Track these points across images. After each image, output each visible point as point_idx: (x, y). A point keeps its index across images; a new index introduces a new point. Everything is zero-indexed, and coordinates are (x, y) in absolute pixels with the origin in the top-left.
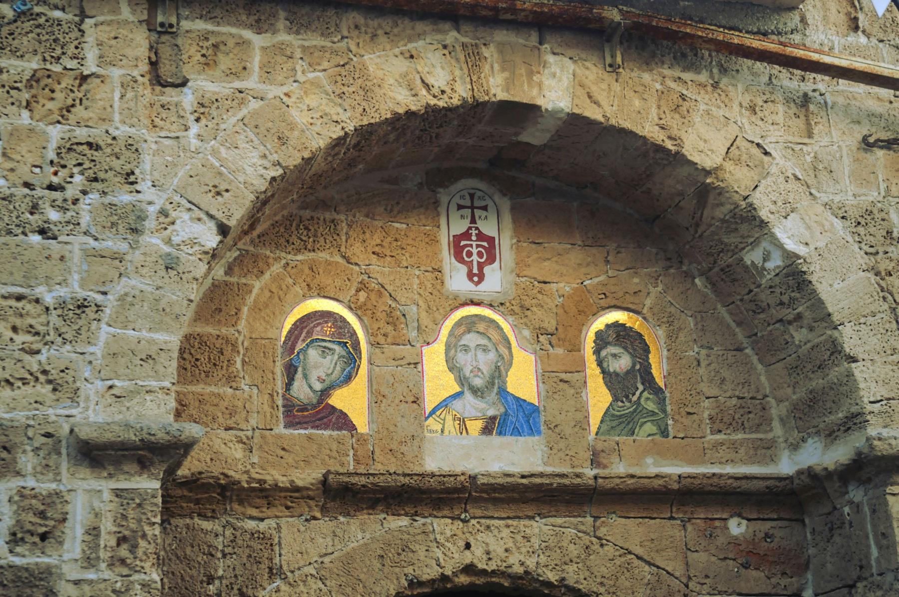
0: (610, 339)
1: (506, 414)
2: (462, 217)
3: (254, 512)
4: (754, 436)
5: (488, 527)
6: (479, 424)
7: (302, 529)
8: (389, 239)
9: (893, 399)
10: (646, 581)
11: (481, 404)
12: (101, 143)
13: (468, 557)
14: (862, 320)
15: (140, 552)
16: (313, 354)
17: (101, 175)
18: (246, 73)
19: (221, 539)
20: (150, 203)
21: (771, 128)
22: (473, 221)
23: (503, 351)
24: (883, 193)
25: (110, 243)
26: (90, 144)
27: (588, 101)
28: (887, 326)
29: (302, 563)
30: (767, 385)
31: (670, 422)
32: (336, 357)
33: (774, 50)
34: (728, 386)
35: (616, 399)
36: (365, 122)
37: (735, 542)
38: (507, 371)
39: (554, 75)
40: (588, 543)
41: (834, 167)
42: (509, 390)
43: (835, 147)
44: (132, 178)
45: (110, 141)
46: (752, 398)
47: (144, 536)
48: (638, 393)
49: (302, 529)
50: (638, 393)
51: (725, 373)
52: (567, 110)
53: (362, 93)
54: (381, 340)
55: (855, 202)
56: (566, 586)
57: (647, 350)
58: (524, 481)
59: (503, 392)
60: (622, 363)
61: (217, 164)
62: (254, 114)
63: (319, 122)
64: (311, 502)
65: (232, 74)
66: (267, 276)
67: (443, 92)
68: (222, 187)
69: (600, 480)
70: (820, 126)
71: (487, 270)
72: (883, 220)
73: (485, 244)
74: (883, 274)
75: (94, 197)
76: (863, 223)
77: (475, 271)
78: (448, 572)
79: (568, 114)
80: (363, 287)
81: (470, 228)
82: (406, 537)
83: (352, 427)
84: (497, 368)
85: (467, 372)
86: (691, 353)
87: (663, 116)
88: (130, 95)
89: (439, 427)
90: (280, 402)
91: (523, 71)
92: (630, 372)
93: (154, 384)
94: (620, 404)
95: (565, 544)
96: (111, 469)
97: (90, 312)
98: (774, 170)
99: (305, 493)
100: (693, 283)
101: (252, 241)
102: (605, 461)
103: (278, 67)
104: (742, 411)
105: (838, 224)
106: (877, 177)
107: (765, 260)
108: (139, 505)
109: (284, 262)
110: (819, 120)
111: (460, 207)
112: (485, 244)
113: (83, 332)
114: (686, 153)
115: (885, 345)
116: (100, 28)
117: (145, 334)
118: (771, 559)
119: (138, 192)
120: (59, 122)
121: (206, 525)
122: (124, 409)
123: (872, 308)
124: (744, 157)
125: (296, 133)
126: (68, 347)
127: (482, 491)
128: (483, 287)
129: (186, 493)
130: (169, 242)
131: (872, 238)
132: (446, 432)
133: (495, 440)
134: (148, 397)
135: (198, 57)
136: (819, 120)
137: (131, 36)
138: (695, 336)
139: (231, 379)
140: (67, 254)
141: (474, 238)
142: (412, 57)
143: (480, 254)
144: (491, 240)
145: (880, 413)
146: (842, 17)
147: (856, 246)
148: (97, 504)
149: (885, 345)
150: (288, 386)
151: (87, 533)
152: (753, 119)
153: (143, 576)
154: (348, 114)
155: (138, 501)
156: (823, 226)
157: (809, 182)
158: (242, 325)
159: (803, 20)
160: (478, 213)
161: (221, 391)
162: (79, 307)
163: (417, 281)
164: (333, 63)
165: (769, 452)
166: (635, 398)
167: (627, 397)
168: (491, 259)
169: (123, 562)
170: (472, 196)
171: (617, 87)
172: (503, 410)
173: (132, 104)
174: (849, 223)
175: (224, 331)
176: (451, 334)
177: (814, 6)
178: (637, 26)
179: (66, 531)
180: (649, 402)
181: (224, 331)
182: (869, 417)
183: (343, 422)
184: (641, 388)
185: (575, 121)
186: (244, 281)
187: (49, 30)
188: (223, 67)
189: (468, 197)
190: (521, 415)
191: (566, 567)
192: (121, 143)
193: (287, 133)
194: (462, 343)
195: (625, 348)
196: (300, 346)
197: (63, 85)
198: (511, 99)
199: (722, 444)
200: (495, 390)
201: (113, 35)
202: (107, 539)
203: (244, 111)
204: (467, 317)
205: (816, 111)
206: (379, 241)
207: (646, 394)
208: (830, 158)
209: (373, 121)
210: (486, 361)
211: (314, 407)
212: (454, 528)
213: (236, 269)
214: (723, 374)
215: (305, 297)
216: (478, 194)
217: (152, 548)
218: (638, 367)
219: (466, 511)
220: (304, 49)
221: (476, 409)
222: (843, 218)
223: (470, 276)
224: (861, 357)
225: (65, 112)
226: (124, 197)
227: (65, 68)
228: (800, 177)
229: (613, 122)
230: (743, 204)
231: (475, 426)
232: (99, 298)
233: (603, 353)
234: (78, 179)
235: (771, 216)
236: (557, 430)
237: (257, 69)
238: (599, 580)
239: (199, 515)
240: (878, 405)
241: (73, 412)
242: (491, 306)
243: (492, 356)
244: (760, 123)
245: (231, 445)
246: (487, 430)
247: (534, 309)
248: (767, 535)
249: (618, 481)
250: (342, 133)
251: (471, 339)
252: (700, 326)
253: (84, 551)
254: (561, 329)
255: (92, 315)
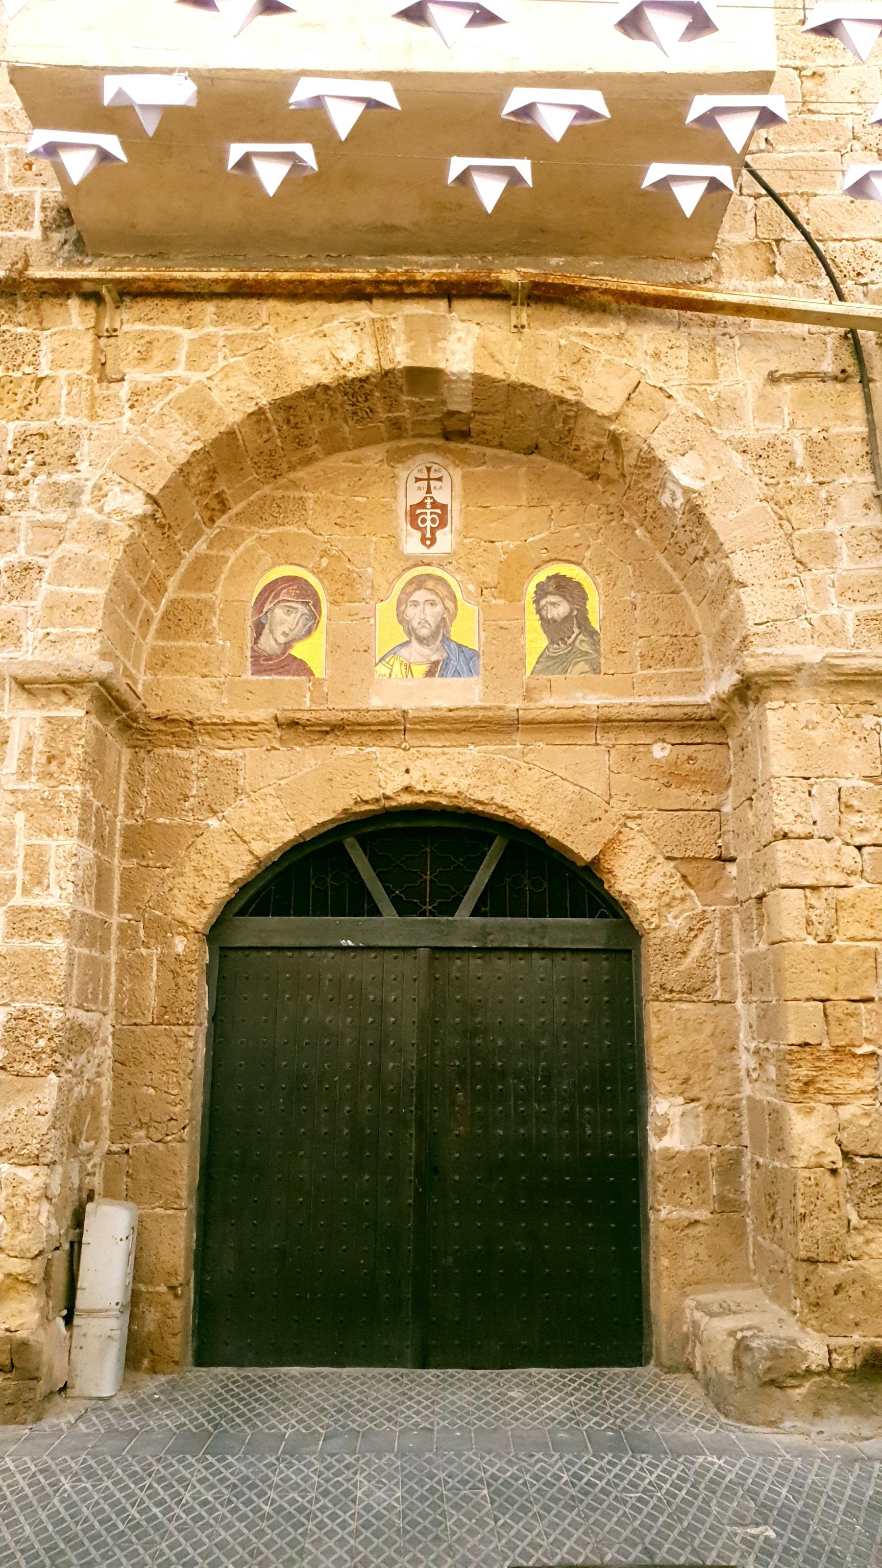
0: (551, 589)
1: (448, 658)
2: (419, 488)
3: (221, 743)
4: (683, 670)
5: (426, 755)
6: (425, 668)
7: (264, 757)
8: (350, 512)
9: (781, 620)
10: (568, 799)
11: (426, 651)
12: (50, 433)
13: (406, 780)
14: (756, 547)
15: (66, 768)
16: (279, 612)
17: (48, 460)
18: (175, 363)
19: (195, 765)
20: (87, 480)
21: (675, 372)
22: (429, 491)
23: (449, 604)
24: (787, 426)
25: (51, 515)
26: (41, 435)
27: (490, 360)
28: (782, 551)
29: (262, 785)
30: (700, 624)
31: (602, 661)
32: (299, 614)
33: (666, 294)
34: (661, 626)
35: (552, 642)
36: (277, 397)
37: (657, 765)
38: (451, 622)
39: (459, 339)
40: (516, 767)
41: (738, 404)
42: (453, 638)
43: (740, 386)
44: (73, 461)
45: (57, 431)
46: (685, 636)
47: (69, 755)
48: (574, 636)
49: (264, 757)
50: (574, 636)
51: (659, 614)
52: (471, 371)
53: (276, 370)
54: (339, 598)
55: (757, 436)
56: (496, 804)
57: (584, 597)
58: (451, 714)
59: (446, 639)
60: (560, 609)
61: (145, 443)
62: (180, 397)
63: (237, 400)
64: (269, 735)
65: (163, 366)
66: (241, 548)
67: (351, 364)
68: (148, 463)
69: (521, 712)
70: (726, 367)
71: (439, 534)
72: (786, 451)
73: (439, 511)
74: (782, 502)
75: (42, 478)
76: (764, 455)
77: (428, 535)
78: (389, 793)
79: (473, 375)
80: (325, 553)
81: (426, 498)
82: (352, 763)
83: (309, 672)
84: (443, 619)
85: (415, 624)
86: (629, 598)
87: (564, 369)
88: (74, 391)
89: (388, 671)
90: (249, 653)
91: (428, 339)
92: (567, 618)
93: (82, 630)
94: (555, 646)
95: (494, 768)
96: (43, 700)
97: (33, 574)
98: (673, 410)
99: (261, 726)
100: (633, 533)
101: (230, 519)
102: (536, 696)
103: (203, 356)
104: (673, 648)
105: (738, 458)
106: (782, 412)
107: (673, 500)
108: (67, 730)
109: (257, 535)
110: (726, 360)
111: (418, 480)
112: (439, 511)
113: (27, 589)
114: (585, 402)
115: (776, 569)
116: (54, 337)
117: (76, 589)
118: (692, 779)
119: (78, 471)
120: (17, 419)
121: (183, 754)
122: (57, 652)
123: (767, 535)
124: (647, 402)
125: (215, 411)
126: (14, 602)
127: (415, 723)
128: (433, 549)
129: (162, 728)
130: (100, 511)
131: (773, 470)
132: (393, 676)
133: (437, 680)
134: (78, 642)
135: (135, 353)
136: (726, 360)
137: (78, 341)
138: (632, 582)
139: (208, 635)
140: (17, 526)
141: (429, 506)
142: (325, 336)
143: (433, 521)
144: (443, 507)
145: (764, 634)
146: (761, 264)
147: (757, 478)
148: (32, 728)
149: (776, 569)
150: (256, 640)
151: (23, 752)
152: (657, 365)
153: (67, 787)
154: (263, 391)
155: (65, 727)
156: (721, 460)
157: (711, 420)
158: (219, 590)
159: (718, 270)
160: (433, 484)
161: (199, 645)
162: (26, 569)
163: (373, 546)
164: (253, 347)
165: (698, 683)
166: (570, 641)
167: (562, 639)
168: (443, 524)
169: (51, 775)
170: (429, 469)
171: (519, 345)
172: (446, 655)
173: (76, 398)
174: (749, 456)
175: (204, 596)
176: (403, 591)
177: (730, 255)
178: (536, 285)
179: (8, 751)
180: (584, 644)
181: (204, 596)
182: (752, 639)
183: (302, 668)
184: (576, 631)
185: (481, 381)
186: (221, 553)
187: (12, 343)
188: (156, 361)
189: (425, 470)
190: (462, 658)
191: (494, 788)
192: (66, 430)
193: (207, 412)
194: (412, 598)
195: (564, 597)
196: (267, 606)
197: (23, 387)
198: (415, 365)
199: (651, 678)
200: (440, 638)
201: (64, 342)
202: (38, 758)
203: (172, 395)
204: (419, 576)
205: (722, 353)
206: (341, 514)
207: (581, 636)
208: (734, 396)
209: (284, 395)
210: (432, 614)
211: (278, 657)
212: (395, 755)
213: (216, 543)
214: (658, 616)
215: (274, 566)
216: (435, 467)
217: (76, 765)
218: (575, 613)
219: (405, 740)
220: (227, 337)
221: (421, 655)
222: (744, 452)
223: (423, 540)
224: (749, 582)
225: (23, 411)
226: (64, 477)
227: (24, 374)
228: (702, 416)
229: (513, 378)
230: (645, 447)
231: (420, 670)
232: (41, 561)
233: (543, 602)
234: (30, 464)
235: (669, 455)
236: (493, 672)
237: (183, 359)
238: (524, 798)
239: (177, 746)
240: (764, 626)
241: (16, 655)
242: (440, 566)
243: (439, 608)
244: (663, 368)
245: (205, 689)
246: (430, 673)
247: (480, 566)
248: (690, 758)
249: (538, 712)
250: (256, 408)
251: (420, 596)
252: (637, 573)
253: (19, 767)
254: (502, 582)
255: (35, 576)
